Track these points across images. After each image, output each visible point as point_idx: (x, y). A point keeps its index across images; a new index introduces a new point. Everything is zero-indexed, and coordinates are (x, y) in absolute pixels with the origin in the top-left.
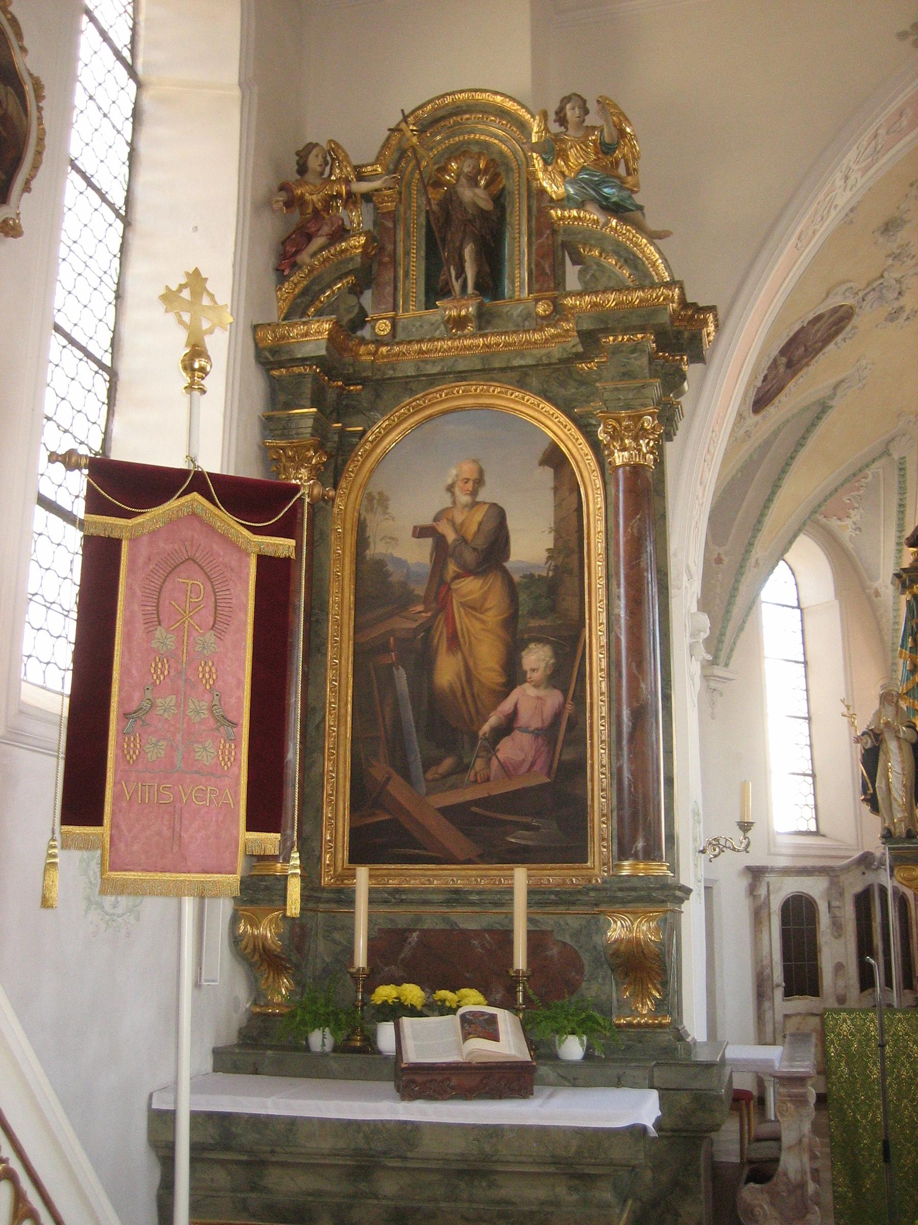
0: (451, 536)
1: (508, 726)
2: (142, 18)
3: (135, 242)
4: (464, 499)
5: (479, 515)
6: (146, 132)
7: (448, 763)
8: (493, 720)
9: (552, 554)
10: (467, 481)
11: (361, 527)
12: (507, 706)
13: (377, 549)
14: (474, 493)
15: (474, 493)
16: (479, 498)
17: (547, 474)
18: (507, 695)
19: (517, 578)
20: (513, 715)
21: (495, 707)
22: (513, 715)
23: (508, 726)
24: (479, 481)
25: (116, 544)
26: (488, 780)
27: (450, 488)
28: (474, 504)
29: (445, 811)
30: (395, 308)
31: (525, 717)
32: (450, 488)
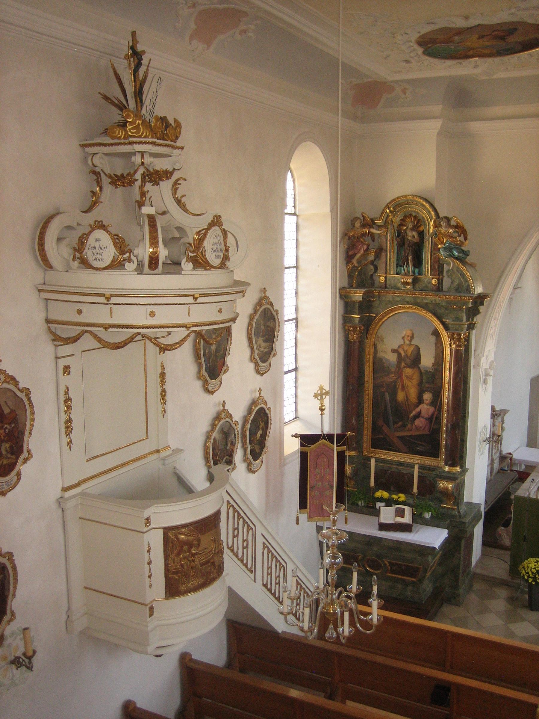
0: (403, 354)
1: (418, 416)
2: (297, 192)
3: (300, 273)
4: (407, 342)
5: (412, 348)
6: (301, 232)
7: (400, 423)
8: (414, 413)
9: (434, 364)
10: (408, 336)
11: (375, 347)
12: (418, 409)
13: (380, 354)
14: (411, 341)
15: (411, 341)
16: (412, 343)
17: (433, 338)
18: (418, 406)
19: (423, 371)
20: (420, 412)
21: (414, 410)
22: (420, 412)
23: (418, 416)
24: (412, 337)
25: (307, 453)
26: (412, 430)
27: (403, 338)
28: (410, 345)
29: (398, 437)
30: (386, 273)
31: (423, 413)
32: (403, 338)
